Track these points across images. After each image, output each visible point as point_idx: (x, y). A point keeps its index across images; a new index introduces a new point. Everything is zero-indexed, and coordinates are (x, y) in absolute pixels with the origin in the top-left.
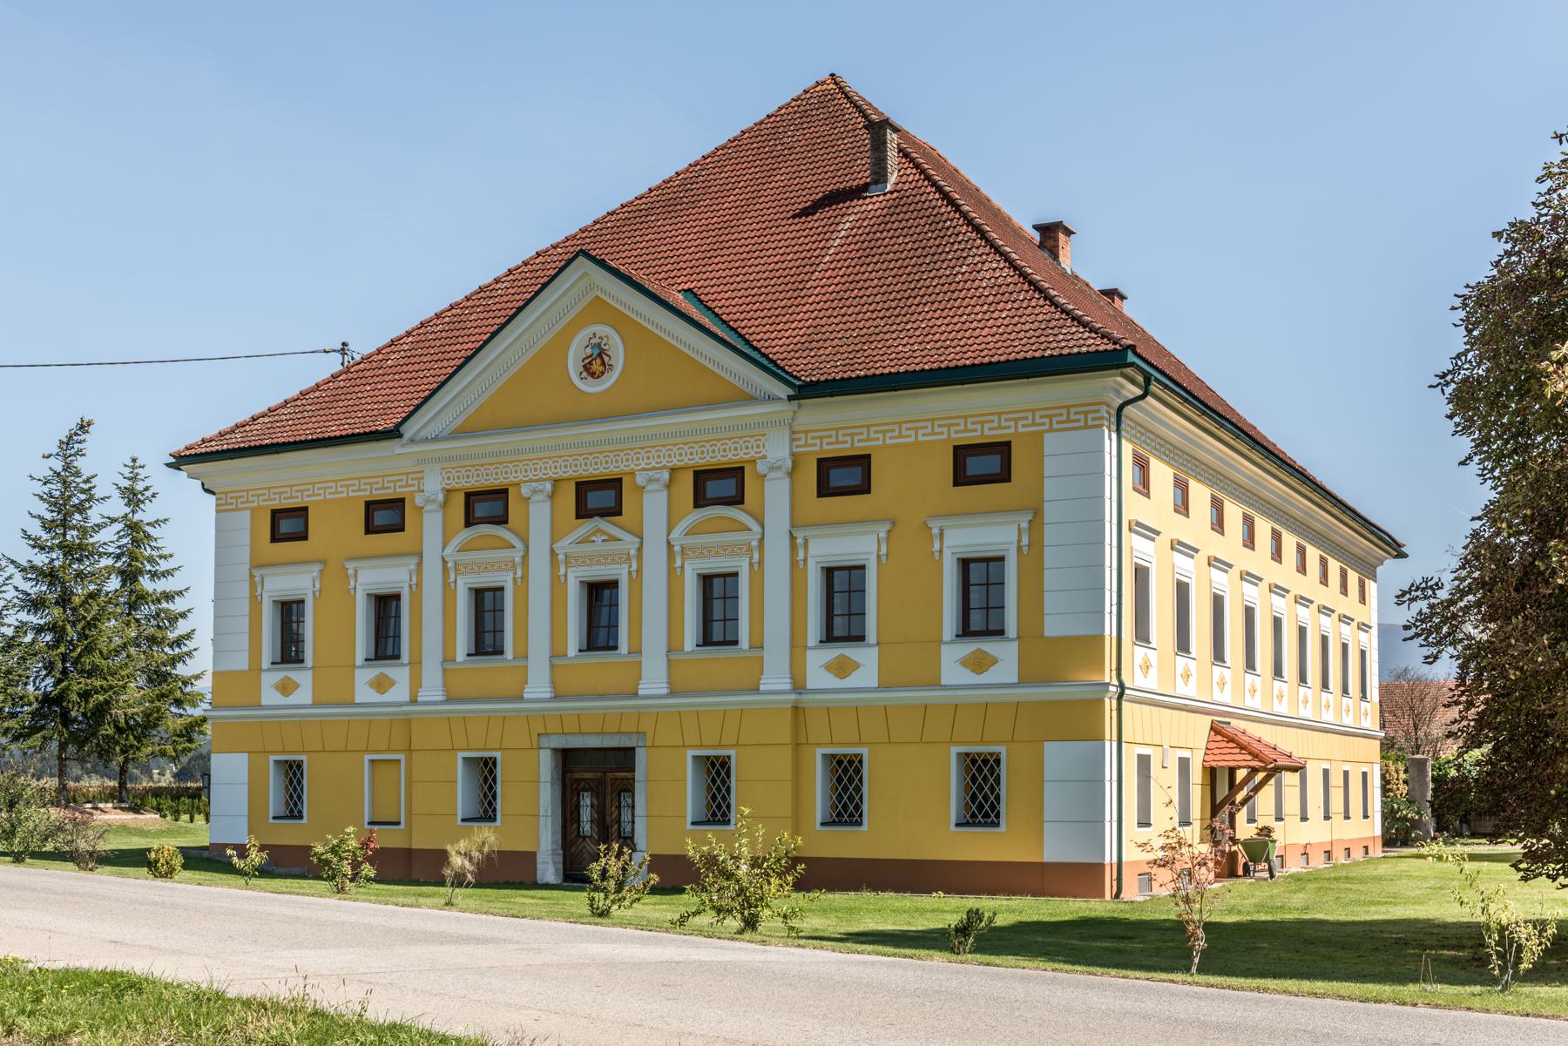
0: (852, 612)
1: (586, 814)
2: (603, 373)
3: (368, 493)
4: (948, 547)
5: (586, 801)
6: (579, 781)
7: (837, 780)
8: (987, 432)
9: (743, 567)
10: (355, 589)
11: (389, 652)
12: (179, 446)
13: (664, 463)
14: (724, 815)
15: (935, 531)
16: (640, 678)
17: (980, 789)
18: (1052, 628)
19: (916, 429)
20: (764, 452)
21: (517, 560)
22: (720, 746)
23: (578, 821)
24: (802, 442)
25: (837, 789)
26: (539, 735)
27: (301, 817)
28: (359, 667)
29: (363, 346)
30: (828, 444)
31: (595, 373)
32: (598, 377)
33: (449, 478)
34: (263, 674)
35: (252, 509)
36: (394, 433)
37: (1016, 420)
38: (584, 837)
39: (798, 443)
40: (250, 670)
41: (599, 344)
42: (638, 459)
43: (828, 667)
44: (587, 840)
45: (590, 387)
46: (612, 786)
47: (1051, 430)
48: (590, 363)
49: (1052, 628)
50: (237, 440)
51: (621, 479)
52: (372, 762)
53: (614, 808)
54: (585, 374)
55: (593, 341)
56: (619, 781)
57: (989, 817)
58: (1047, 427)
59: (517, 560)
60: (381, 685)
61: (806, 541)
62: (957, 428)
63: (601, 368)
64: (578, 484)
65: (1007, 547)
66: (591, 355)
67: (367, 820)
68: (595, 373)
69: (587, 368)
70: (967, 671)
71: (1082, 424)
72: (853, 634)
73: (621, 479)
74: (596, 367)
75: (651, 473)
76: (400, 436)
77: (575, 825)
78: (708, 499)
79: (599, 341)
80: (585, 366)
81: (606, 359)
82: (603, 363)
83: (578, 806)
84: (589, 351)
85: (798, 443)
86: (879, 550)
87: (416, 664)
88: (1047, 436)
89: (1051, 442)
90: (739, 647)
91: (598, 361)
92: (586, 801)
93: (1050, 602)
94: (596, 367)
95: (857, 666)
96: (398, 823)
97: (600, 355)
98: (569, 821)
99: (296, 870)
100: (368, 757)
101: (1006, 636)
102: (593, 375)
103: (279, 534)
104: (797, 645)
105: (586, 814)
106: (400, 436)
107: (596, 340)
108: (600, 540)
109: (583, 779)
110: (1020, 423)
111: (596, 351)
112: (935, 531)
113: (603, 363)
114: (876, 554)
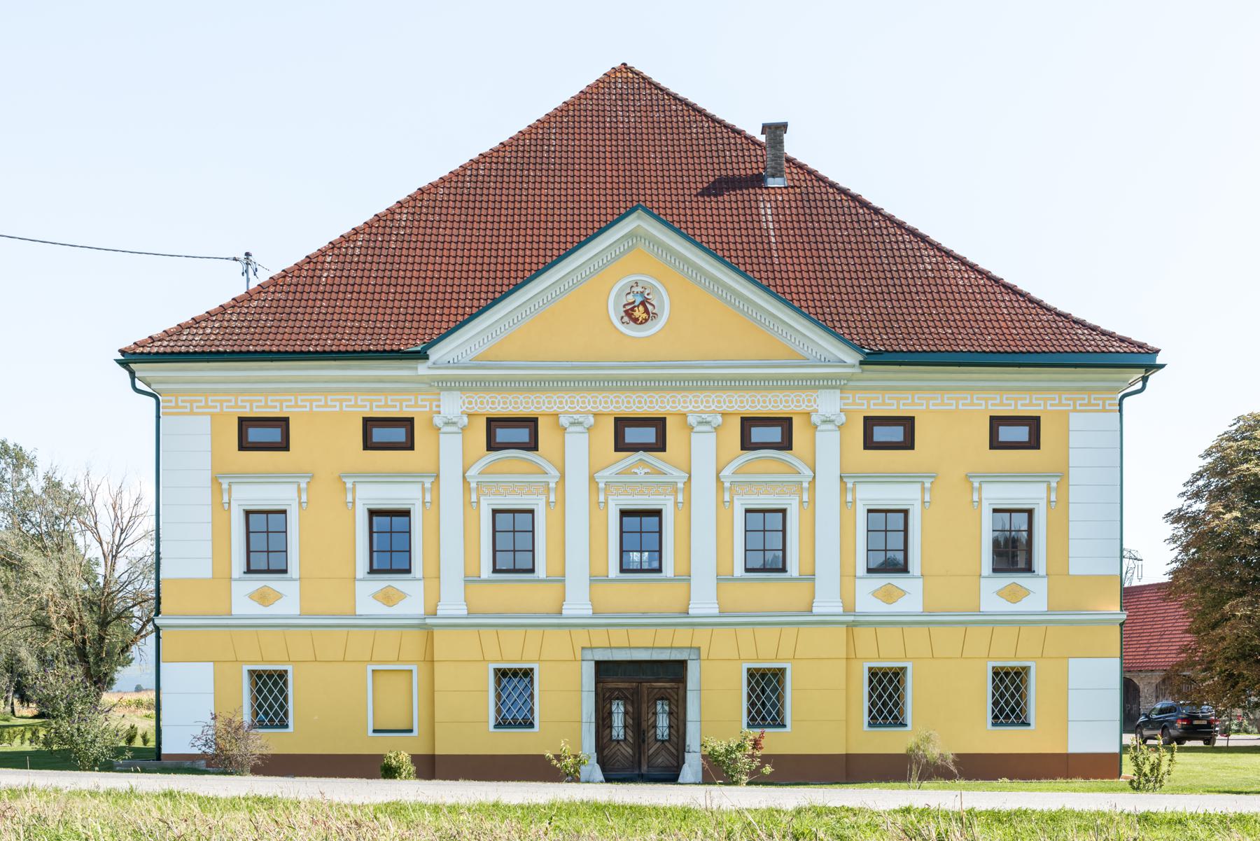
0: (389, 553)
1: (618, 720)
2: (646, 320)
3: (367, 409)
4: (986, 499)
5: (618, 710)
6: (612, 690)
7: (899, 690)
8: (1020, 407)
9: (538, 503)
10: (229, 503)
11: (1022, 565)
12: (127, 343)
13: (713, 407)
14: (281, 720)
15: (225, 486)
16: (814, 598)
17: (265, 699)
18: (1076, 568)
19: (401, 401)
20: (815, 406)
21: (552, 485)
22: (521, 661)
23: (611, 727)
24: (851, 401)
25: (898, 697)
26: (583, 648)
27: (287, 726)
28: (236, 580)
29: (273, 263)
30: (406, 406)
31: (638, 319)
32: (641, 323)
33: (470, 403)
34: (234, 583)
35: (212, 415)
36: (422, 356)
37: (311, 401)
38: (618, 741)
39: (846, 401)
40: (213, 578)
41: (642, 293)
42: (685, 402)
43: (875, 594)
44: (622, 743)
45: (631, 331)
46: (648, 696)
47: (1075, 411)
48: (632, 309)
49: (1076, 568)
50: (196, 342)
51: (665, 418)
52: (373, 671)
53: (650, 715)
54: (626, 319)
55: (635, 289)
56: (656, 691)
57: (767, 720)
58: (1071, 408)
59: (552, 485)
60: (263, 598)
61: (230, 484)
62: (259, 404)
63: (645, 315)
64: (743, 419)
65: (1037, 501)
66: (634, 302)
67: (370, 729)
68: (638, 319)
69: (629, 313)
70: (255, 604)
71: (188, 410)
72: (517, 567)
73: (665, 418)
74: (639, 313)
75: (575, 416)
76: (426, 357)
77: (653, 731)
78: (1001, 442)
79: (642, 290)
80: (626, 312)
81: (650, 308)
82: (646, 311)
83: (611, 713)
84: (631, 298)
85: (846, 401)
86: (300, 498)
87: (434, 577)
88: (1072, 415)
89: (1076, 421)
90: (536, 574)
91: (641, 308)
92: (618, 710)
93: (1075, 548)
94: (639, 313)
95: (903, 593)
96: (411, 731)
97: (643, 303)
98: (601, 727)
99: (792, 782)
100: (370, 668)
101: (1036, 573)
102: (635, 320)
103: (406, 443)
104: (847, 575)
105: (618, 720)
106: (426, 357)
107: (639, 289)
108: (643, 472)
109: (617, 689)
110: (990, 402)
111: (639, 300)
112: (349, 485)
113: (646, 311)
114: (421, 500)
